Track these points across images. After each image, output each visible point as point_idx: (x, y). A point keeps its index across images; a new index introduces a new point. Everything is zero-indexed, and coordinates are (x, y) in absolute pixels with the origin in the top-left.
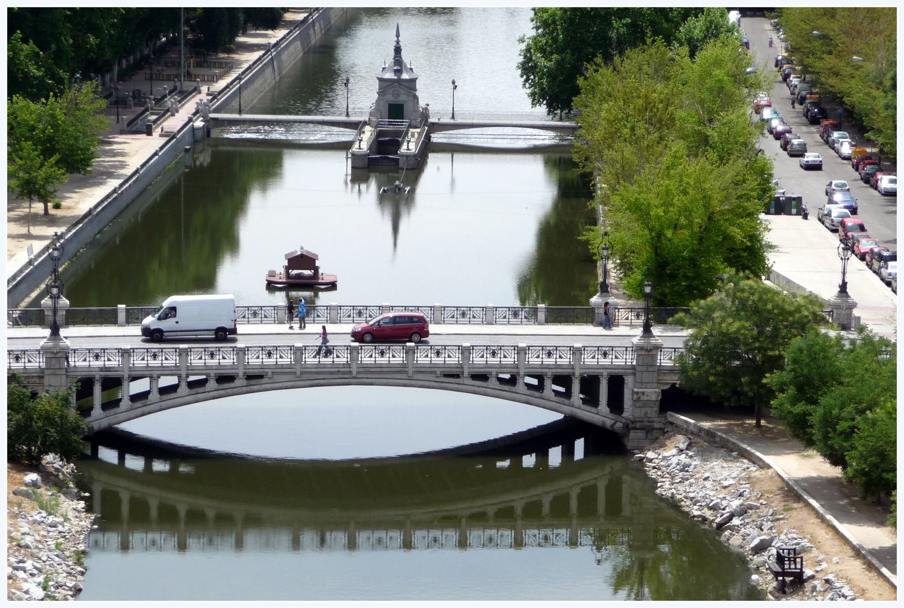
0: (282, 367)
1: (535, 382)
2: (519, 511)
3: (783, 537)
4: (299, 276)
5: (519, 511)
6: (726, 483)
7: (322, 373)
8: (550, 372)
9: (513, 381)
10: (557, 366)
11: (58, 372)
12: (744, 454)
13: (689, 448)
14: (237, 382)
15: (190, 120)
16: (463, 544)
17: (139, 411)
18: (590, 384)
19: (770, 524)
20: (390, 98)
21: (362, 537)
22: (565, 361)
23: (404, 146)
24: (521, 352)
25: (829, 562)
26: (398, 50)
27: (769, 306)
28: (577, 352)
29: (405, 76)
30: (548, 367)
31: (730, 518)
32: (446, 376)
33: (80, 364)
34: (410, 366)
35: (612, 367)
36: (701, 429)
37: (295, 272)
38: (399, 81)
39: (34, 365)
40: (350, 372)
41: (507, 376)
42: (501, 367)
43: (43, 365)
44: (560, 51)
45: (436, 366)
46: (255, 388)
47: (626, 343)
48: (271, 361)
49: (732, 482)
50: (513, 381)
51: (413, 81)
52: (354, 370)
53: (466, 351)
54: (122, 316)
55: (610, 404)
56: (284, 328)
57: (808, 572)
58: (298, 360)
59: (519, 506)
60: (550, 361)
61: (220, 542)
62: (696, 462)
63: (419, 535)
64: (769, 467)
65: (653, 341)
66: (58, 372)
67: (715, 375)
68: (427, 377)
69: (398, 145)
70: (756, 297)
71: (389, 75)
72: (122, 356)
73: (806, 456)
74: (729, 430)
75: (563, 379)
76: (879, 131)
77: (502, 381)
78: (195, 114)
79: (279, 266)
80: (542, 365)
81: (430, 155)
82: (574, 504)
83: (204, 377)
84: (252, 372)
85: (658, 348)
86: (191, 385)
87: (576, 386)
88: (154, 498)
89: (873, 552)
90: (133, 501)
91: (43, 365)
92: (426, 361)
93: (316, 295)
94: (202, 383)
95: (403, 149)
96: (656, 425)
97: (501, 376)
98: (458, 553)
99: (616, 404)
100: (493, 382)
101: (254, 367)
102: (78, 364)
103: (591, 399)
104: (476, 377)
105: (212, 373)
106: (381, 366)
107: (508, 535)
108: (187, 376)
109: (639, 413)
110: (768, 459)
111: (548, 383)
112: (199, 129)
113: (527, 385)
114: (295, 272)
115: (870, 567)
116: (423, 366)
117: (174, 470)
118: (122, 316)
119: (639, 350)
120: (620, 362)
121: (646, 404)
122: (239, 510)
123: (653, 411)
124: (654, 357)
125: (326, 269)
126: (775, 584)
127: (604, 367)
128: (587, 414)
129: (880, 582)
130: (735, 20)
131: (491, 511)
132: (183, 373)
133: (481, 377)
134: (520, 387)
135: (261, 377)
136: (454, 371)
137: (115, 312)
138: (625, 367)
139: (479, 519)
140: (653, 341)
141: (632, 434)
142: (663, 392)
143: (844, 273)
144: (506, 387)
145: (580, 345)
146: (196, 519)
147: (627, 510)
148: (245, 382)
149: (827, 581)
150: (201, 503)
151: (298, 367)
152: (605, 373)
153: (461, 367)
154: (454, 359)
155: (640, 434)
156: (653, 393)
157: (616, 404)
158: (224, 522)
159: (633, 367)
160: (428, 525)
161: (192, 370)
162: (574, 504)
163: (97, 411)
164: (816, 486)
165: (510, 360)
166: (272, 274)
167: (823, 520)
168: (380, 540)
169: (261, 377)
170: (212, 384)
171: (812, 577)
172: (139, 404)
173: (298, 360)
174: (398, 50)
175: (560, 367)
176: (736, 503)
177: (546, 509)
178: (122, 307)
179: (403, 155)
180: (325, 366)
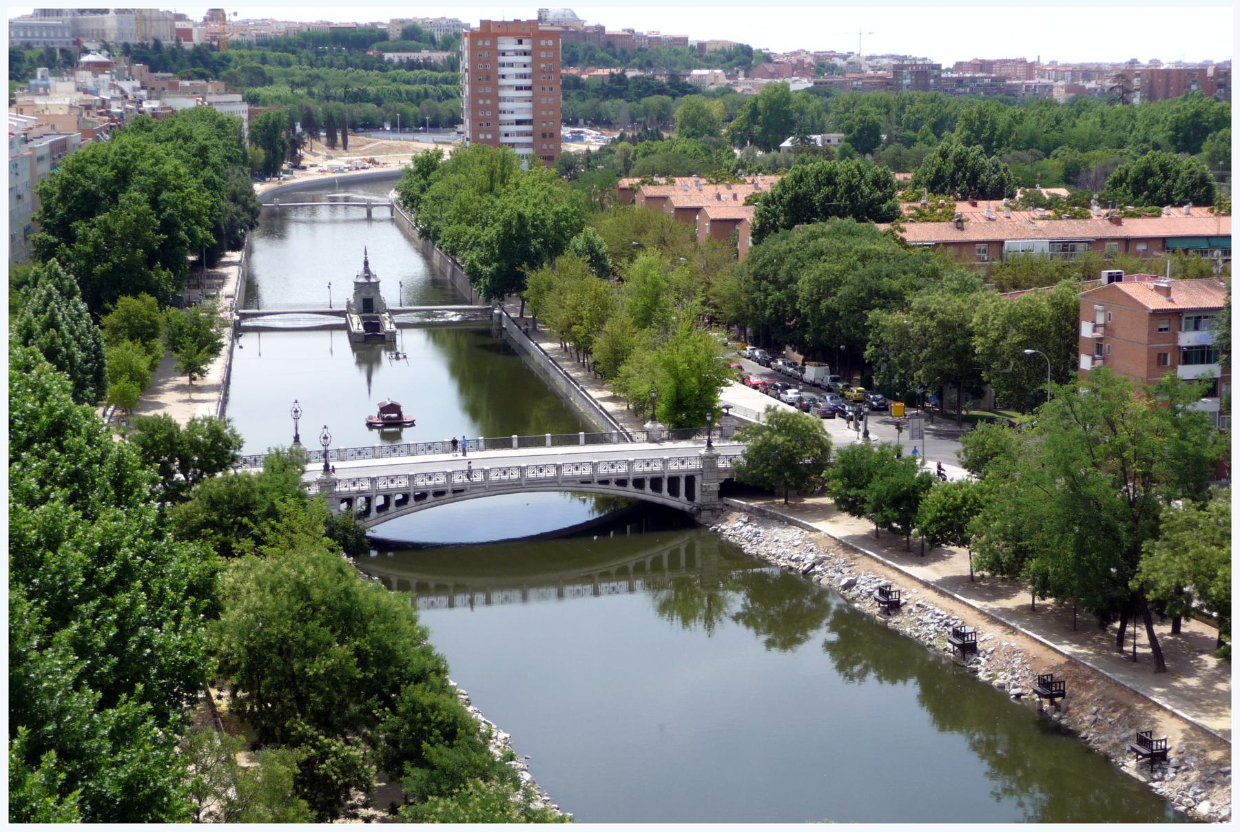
2: (631, 569)
3: (862, 577)
4: (389, 418)
5: (631, 569)
6: (796, 543)
8: (649, 477)
10: (618, 474)
12: (792, 523)
13: (749, 520)
14: (447, 495)
16: (596, 593)
17: (383, 519)
18: (673, 481)
19: (848, 569)
20: (364, 295)
21: (568, 589)
22: (658, 468)
25: (911, 592)
26: (366, 263)
27: (800, 426)
29: (373, 280)
31: (813, 566)
32: (582, 483)
36: (752, 508)
37: (386, 416)
38: (369, 283)
44: (497, 261)
45: (576, 477)
49: (799, 542)
51: (378, 283)
52: (523, 483)
53: (594, 466)
54: (515, 443)
55: (687, 495)
56: (450, 456)
57: (903, 600)
58: (486, 478)
59: (631, 566)
60: (683, 467)
62: (762, 530)
64: (819, 531)
65: (714, 452)
67: (768, 472)
68: (571, 484)
70: (791, 421)
71: (362, 280)
73: (833, 522)
74: (768, 506)
79: (375, 412)
80: (609, 474)
82: (665, 562)
84: (457, 488)
85: (717, 456)
89: (938, 582)
92: (569, 474)
93: (401, 430)
96: (718, 507)
99: (690, 495)
101: (458, 484)
103: (674, 491)
106: (540, 479)
107: (624, 584)
109: (706, 500)
110: (814, 525)
114: (386, 416)
115: (942, 593)
116: (567, 477)
118: (515, 443)
120: (692, 467)
121: (711, 493)
122: (450, 581)
123: (715, 498)
125: (407, 415)
126: (879, 609)
127: (683, 471)
129: (957, 603)
131: (613, 570)
135: (462, 491)
136: (588, 479)
137: (545, 438)
138: (695, 470)
139: (606, 576)
140: (714, 452)
141: (704, 514)
142: (721, 484)
143: (296, 429)
147: (699, 564)
148: (452, 495)
149: (918, 605)
150: (425, 577)
152: (684, 475)
153: (592, 476)
154: (587, 471)
155: (708, 513)
156: (715, 486)
157: (690, 495)
158: (440, 589)
159: (701, 470)
160: (573, 582)
162: (665, 562)
164: (864, 540)
166: (371, 418)
167: (884, 564)
169: (462, 491)
170: (430, 498)
171: (906, 603)
173: (486, 478)
174: (366, 263)
175: (620, 474)
176: (811, 556)
177: (648, 566)
178: (548, 435)
180: (504, 481)
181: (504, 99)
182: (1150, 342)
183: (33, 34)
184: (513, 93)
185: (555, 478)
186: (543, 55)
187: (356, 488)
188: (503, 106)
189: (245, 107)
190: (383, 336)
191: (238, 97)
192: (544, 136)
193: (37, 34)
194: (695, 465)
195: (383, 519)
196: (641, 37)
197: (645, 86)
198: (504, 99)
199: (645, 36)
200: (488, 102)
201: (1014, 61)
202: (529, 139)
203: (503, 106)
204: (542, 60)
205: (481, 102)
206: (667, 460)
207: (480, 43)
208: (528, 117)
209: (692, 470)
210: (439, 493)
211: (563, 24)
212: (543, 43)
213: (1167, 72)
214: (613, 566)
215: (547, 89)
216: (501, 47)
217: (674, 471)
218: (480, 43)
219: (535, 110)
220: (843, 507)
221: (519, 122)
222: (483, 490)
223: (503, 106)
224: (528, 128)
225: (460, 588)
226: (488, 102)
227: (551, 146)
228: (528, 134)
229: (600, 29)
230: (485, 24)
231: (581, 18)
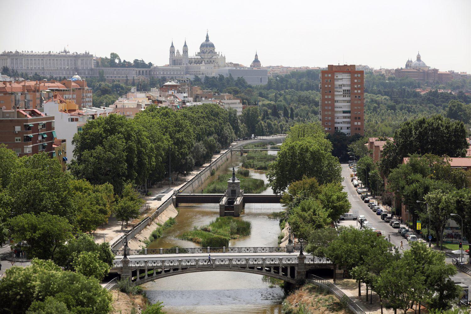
0: (226, 265)
7: (205, 267)
9: (261, 269)
10: (275, 264)
11: (126, 268)
14: (179, 270)
15: (172, 196)
23: (235, 203)
24: (264, 260)
28: (281, 260)
30: (272, 264)
32: (241, 268)
33: (133, 265)
34: (146, 267)
35: (291, 264)
39: (119, 266)
40: (213, 267)
41: (260, 267)
42: (258, 265)
43: (122, 266)
46: (184, 272)
47: (296, 257)
48: (155, 265)
50: (261, 269)
52: (214, 266)
53: (247, 260)
55: (291, 275)
66: (126, 268)
68: (236, 268)
69: (234, 202)
72: (162, 262)
75: (276, 268)
76: (179, 99)
77: (258, 269)
78: (173, 194)
80: (270, 264)
81: (246, 204)
83: (169, 269)
86: (166, 271)
87: (280, 270)
91: (122, 266)
94: (169, 271)
95: (235, 203)
97: (258, 267)
99: (293, 275)
100: (256, 269)
101: (184, 266)
102: (132, 265)
104: (250, 268)
105: (172, 268)
106: (222, 265)
108: (164, 269)
112: (174, 199)
113: (266, 270)
116: (234, 265)
119: (299, 258)
120: (293, 262)
124: (303, 261)
130: (155, 66)
132: (163, 268)
134: (264, 271)
135: (186, 269)
144: (259, 271)
145: (281, 258)
151: (180, 266)
153: (245, 265)
157: (293, 275)
159: (297, 264)
161: (166, 267)
170: (172, 271)
172: (150, 277)
175: (275, 264)
179: (235, 205)
180: (205, 265)
181: (337, 101)
183: (167, 73)
184: (341, 98)
185: (228, 265)
188: (336, 104)
189: (241, 105)
190: (233, 207)
191: (238, 101)
192: (356, 118)
193: (169, 73)
194: (295, 262)
195: (150, 279)
196: (457, 74)
197: (446, 98)
198: (337, 101)
199: (459, 75)
200: (330, 102)
201: (286, 67)
205: (326, 102)
206: (264, 259)
207: (326, 75)
209: (293, 264)
211: (417, 68)
212: (356, 75)
213: (442, 74)
215: (357, 97)
218: (326, 75)
219: (352, 106)
221: (344, 112)
222: (194, 269)
223: (336, 104)
226: (330, 102)
227: (359, 123)
228: (348, 117)
229: (436, 71)
230: (331, 67)
231: (428, 65)
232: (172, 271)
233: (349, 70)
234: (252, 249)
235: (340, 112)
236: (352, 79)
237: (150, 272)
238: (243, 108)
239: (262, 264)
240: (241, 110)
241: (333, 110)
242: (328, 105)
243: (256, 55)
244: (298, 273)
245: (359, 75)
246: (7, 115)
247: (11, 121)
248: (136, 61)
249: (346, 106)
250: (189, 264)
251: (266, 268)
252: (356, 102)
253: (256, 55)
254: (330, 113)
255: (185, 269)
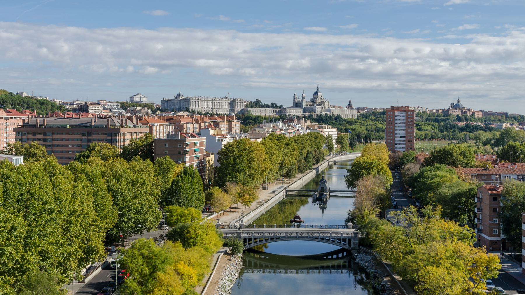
1: (334, 240)
9: (329, 240)
14: (275, 239)
42: (326, 237)
45: (313, 236)
61: (420, 287)
63: (299, 271)
75: (339, 239)
77: (327, 240)
87: (342, 240)
88: (258, 262)
90: (249, 261)
98: (330, 275)
103: (250, 262)
104: (321, 239)
111: (336, 240)
113: (332, 241)
117: (265, 257)
120: (350, 236)
123: (357, 246)
124: (357, 235)
128: (345, 247)
133: (322, 239)
134: (330, 241)
146: (267, 267)
153: (318, 237)
154: (317, 235)
156: (357, 242)
158: (272, 267)
160: (290, 269)
163: (247, 245)
165: (328, 235)
168: (292, 272)
181: (396, 130)
182: (490, 204)
186: (409, 116)
187: (248, 235)
189: (337, 133)
191: (335, 130)
202: (404, 142)
203: (396, 132)
204: (409, 118)
208: (404, 135)
209: (350, 237)
210: (272, 239)
214: (302, 266)
216: (396, 114)
217: (344, 237)
219: (406, 133)
220: (491, 248)
221: (401, 137)
223: (396, 132)
224: (404, 139)
225: (278, 268)
232: (269, 240)
233: (406, 110)
234: (325, 226)
235: (398, 137)
236: (407, 116)
237: (255, 241)
238: (338, 134)
239: (329, 237)
240: (336, 135)
241: (393, 136)
242: (391, 133)
243: (350, 101)
244: (354, 243)
245: (411, 113)
246: (174, 137)
247: (176, 140)
248: (272, 104)
249: (402, 133)
250: (281, 235)
251: (332, 239)
252: (409, 130)
253: (350, 101)
254: (392, 137)
255: (278, 239)
